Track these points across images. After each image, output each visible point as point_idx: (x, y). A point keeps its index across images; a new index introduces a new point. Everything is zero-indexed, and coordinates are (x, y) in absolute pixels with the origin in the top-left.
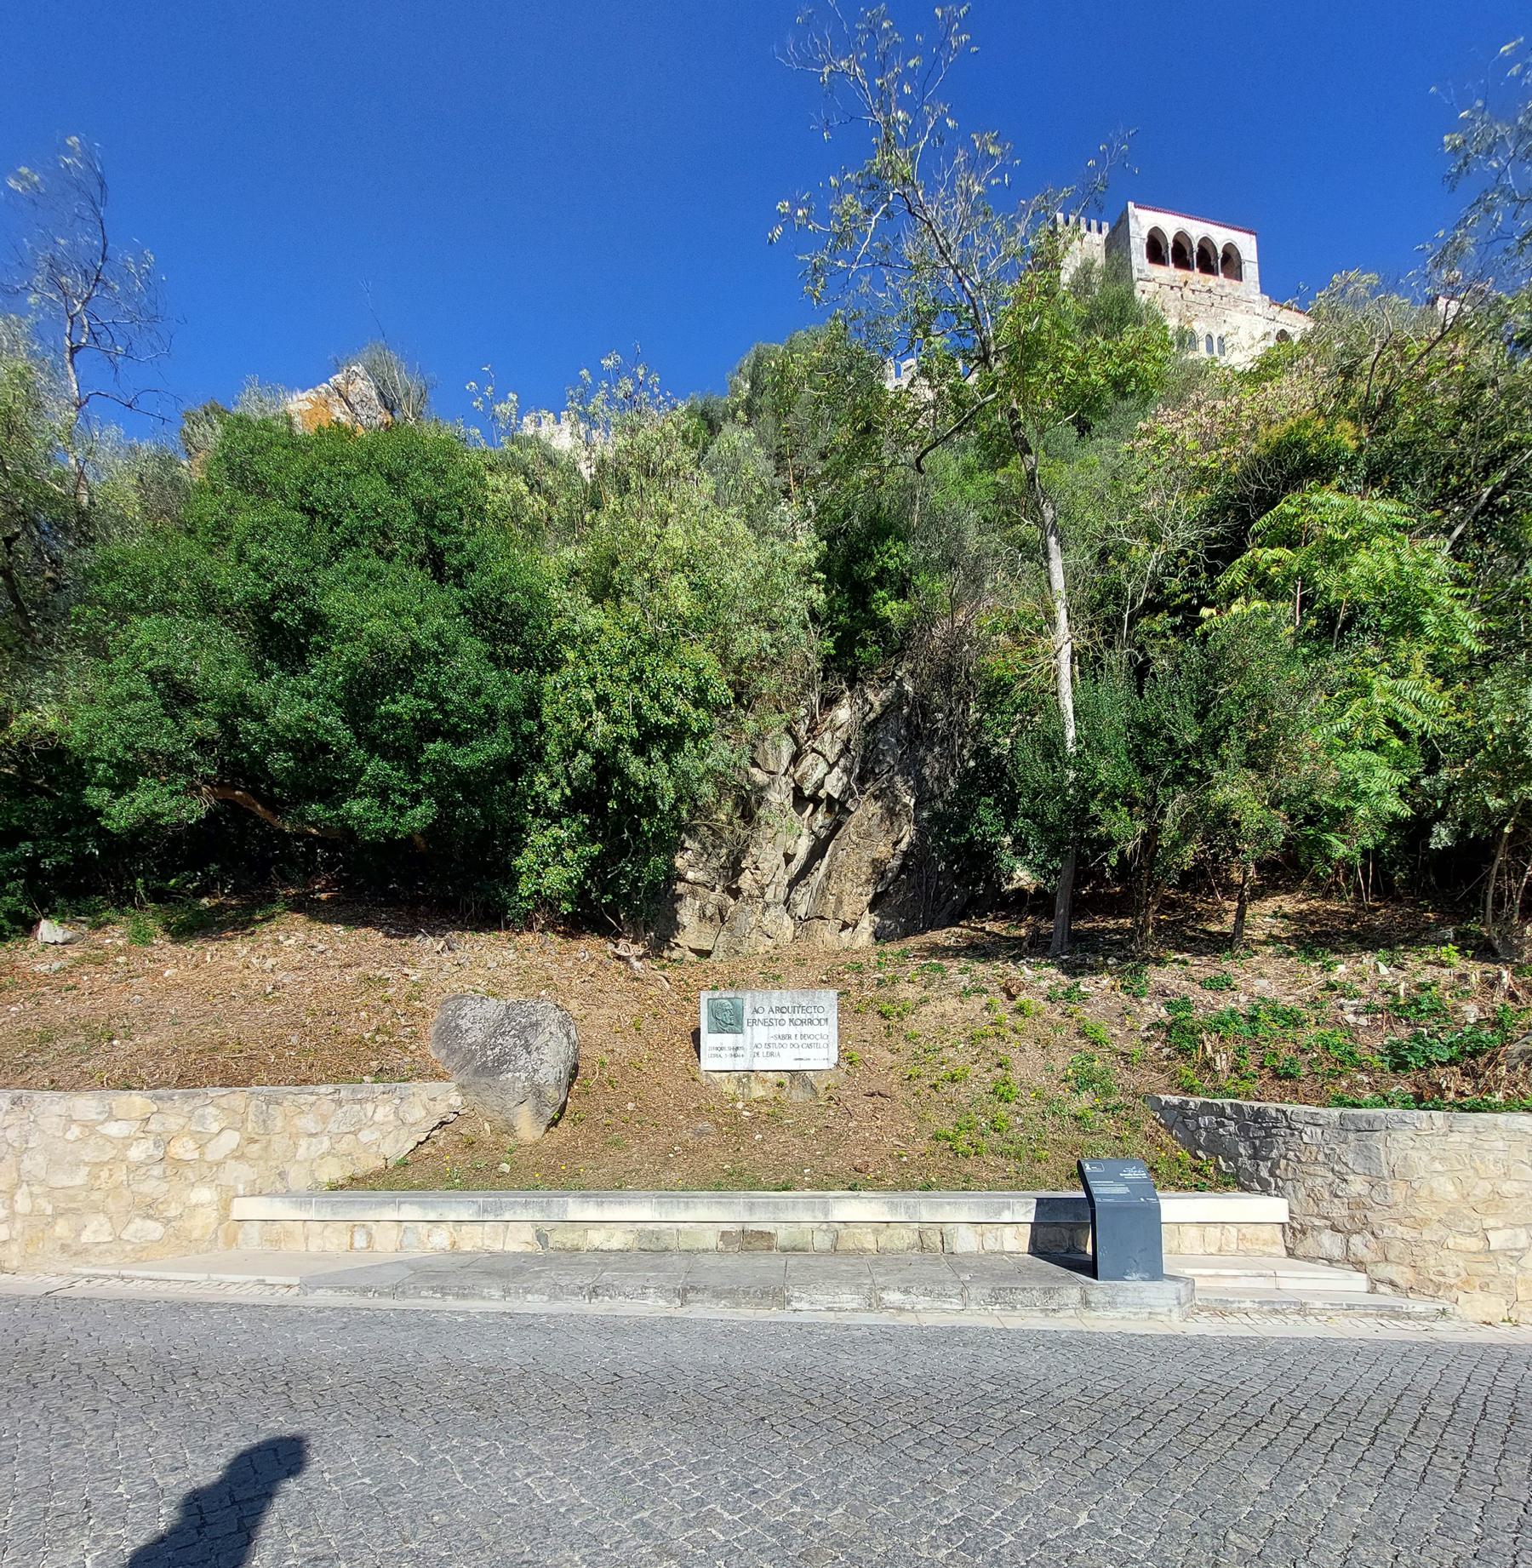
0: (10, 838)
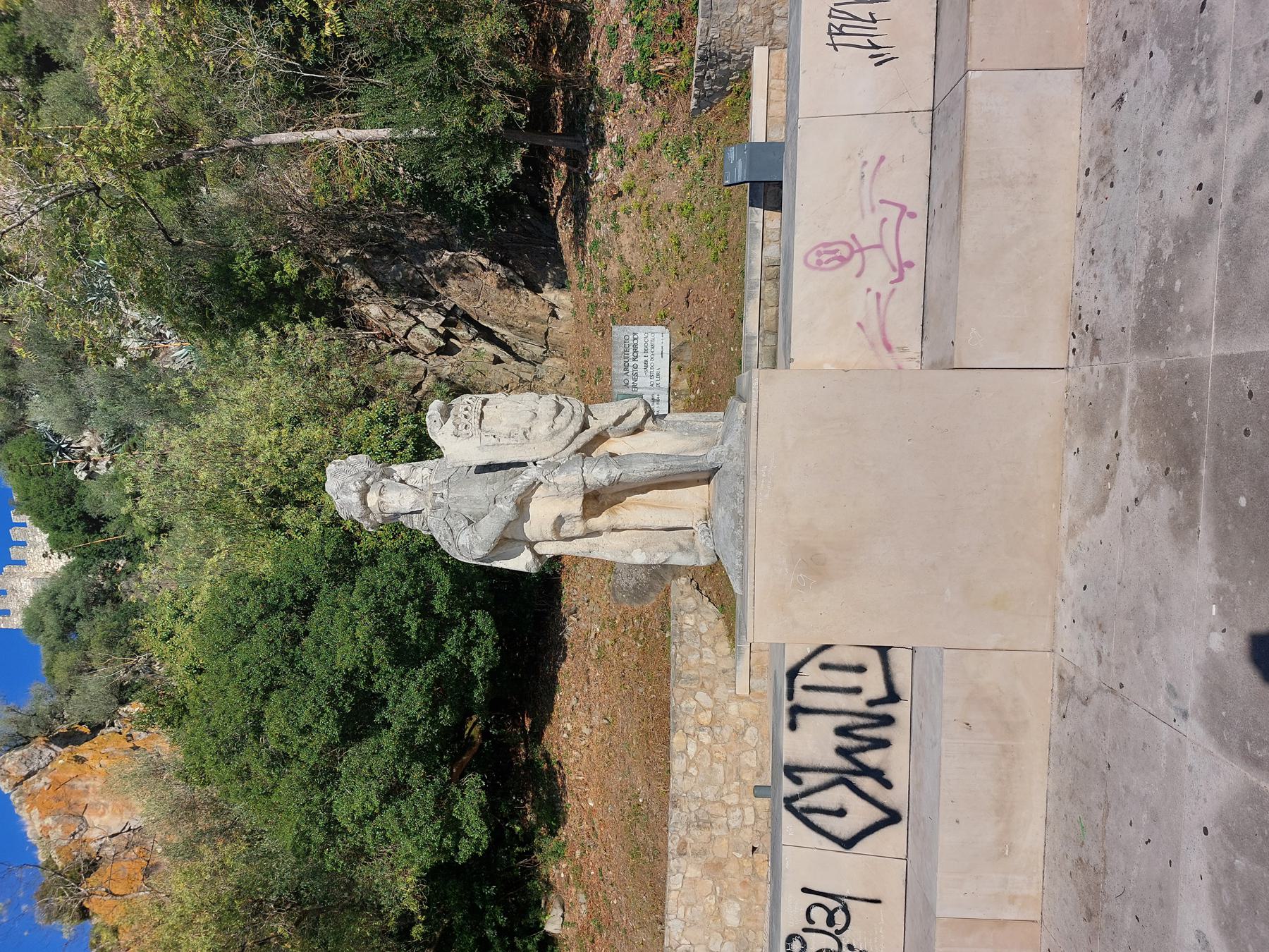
0: (484, 944)
